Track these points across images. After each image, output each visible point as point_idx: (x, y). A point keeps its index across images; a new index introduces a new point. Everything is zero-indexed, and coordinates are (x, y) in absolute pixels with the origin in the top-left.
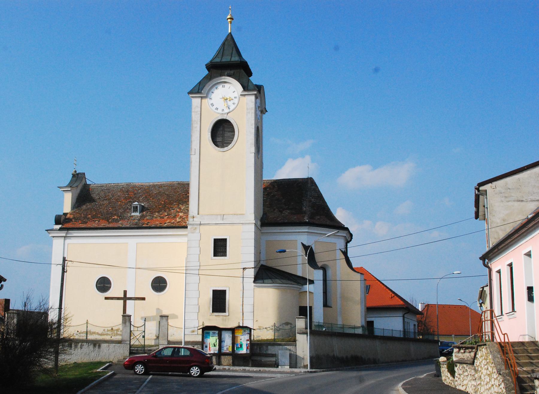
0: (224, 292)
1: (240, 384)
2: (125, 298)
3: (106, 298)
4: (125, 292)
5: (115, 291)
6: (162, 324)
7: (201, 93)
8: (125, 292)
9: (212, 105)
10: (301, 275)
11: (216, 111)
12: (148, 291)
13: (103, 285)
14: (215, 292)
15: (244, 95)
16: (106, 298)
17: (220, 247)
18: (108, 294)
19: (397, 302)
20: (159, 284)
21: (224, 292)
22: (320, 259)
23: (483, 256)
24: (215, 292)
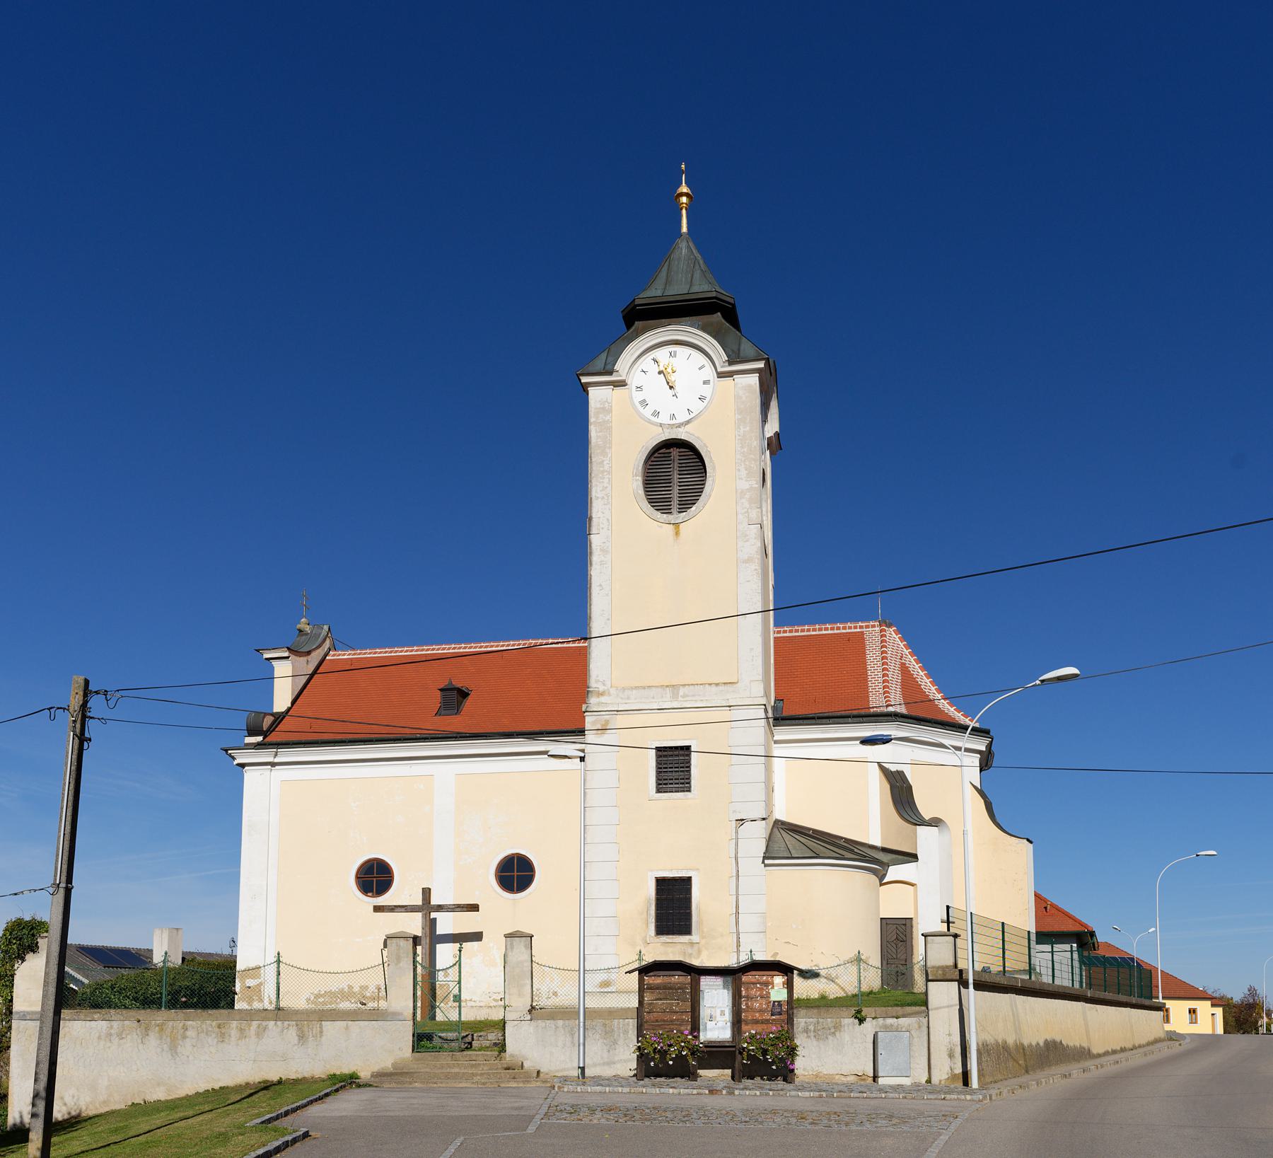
0: (686, 882)
1: (904, 669)
2: (427, 906)
3: (377, 909)
4: (426, 893)
5: (402, 891)
6: (513, 958)
7: (610, 373)
8: (426, 893)
9: (644, 403)
10: (878, 843)
11: (654, 419)
12: (488, 890)
13: (375, 877)
14: (662, 883)
15: (730, 374)
16: (377, 909)
17: (673, 767)
18: (383, 900)
19: (1070, 927)
20: (515, 874)
21: (686, 882)
22: (925, 805)
23: (772, 1076)
24: (662, 883)
